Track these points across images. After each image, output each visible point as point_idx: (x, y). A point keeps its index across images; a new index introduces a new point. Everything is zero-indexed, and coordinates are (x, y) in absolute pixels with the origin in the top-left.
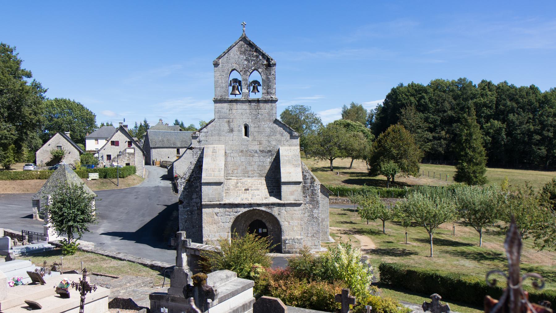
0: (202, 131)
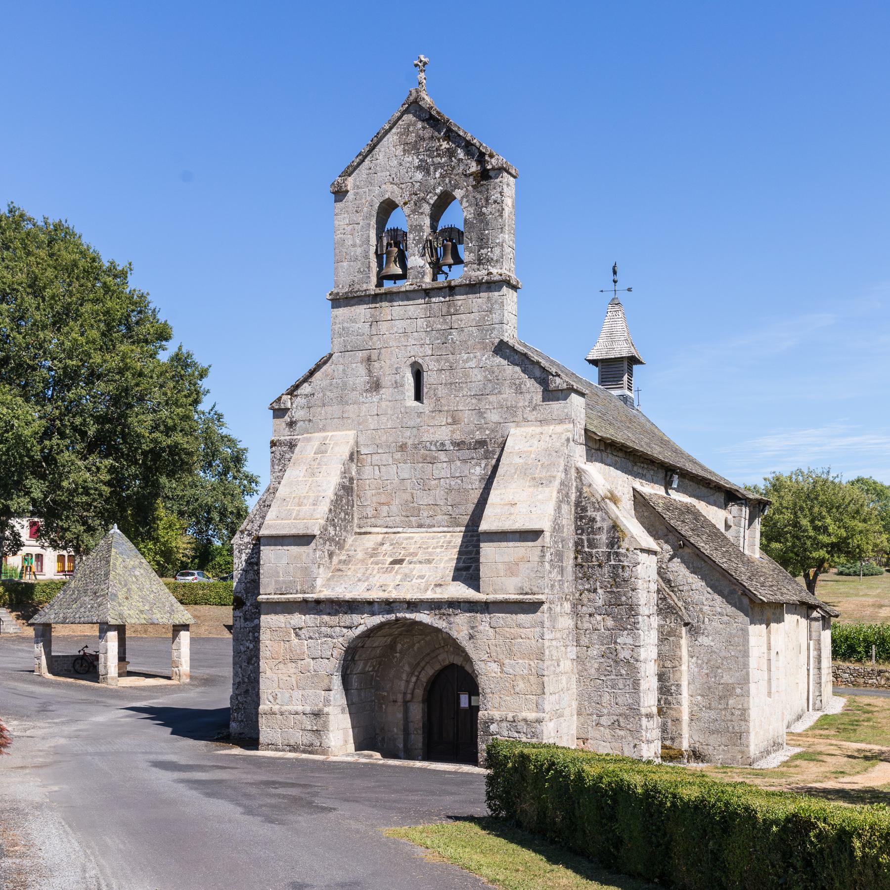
0: (299, 392)
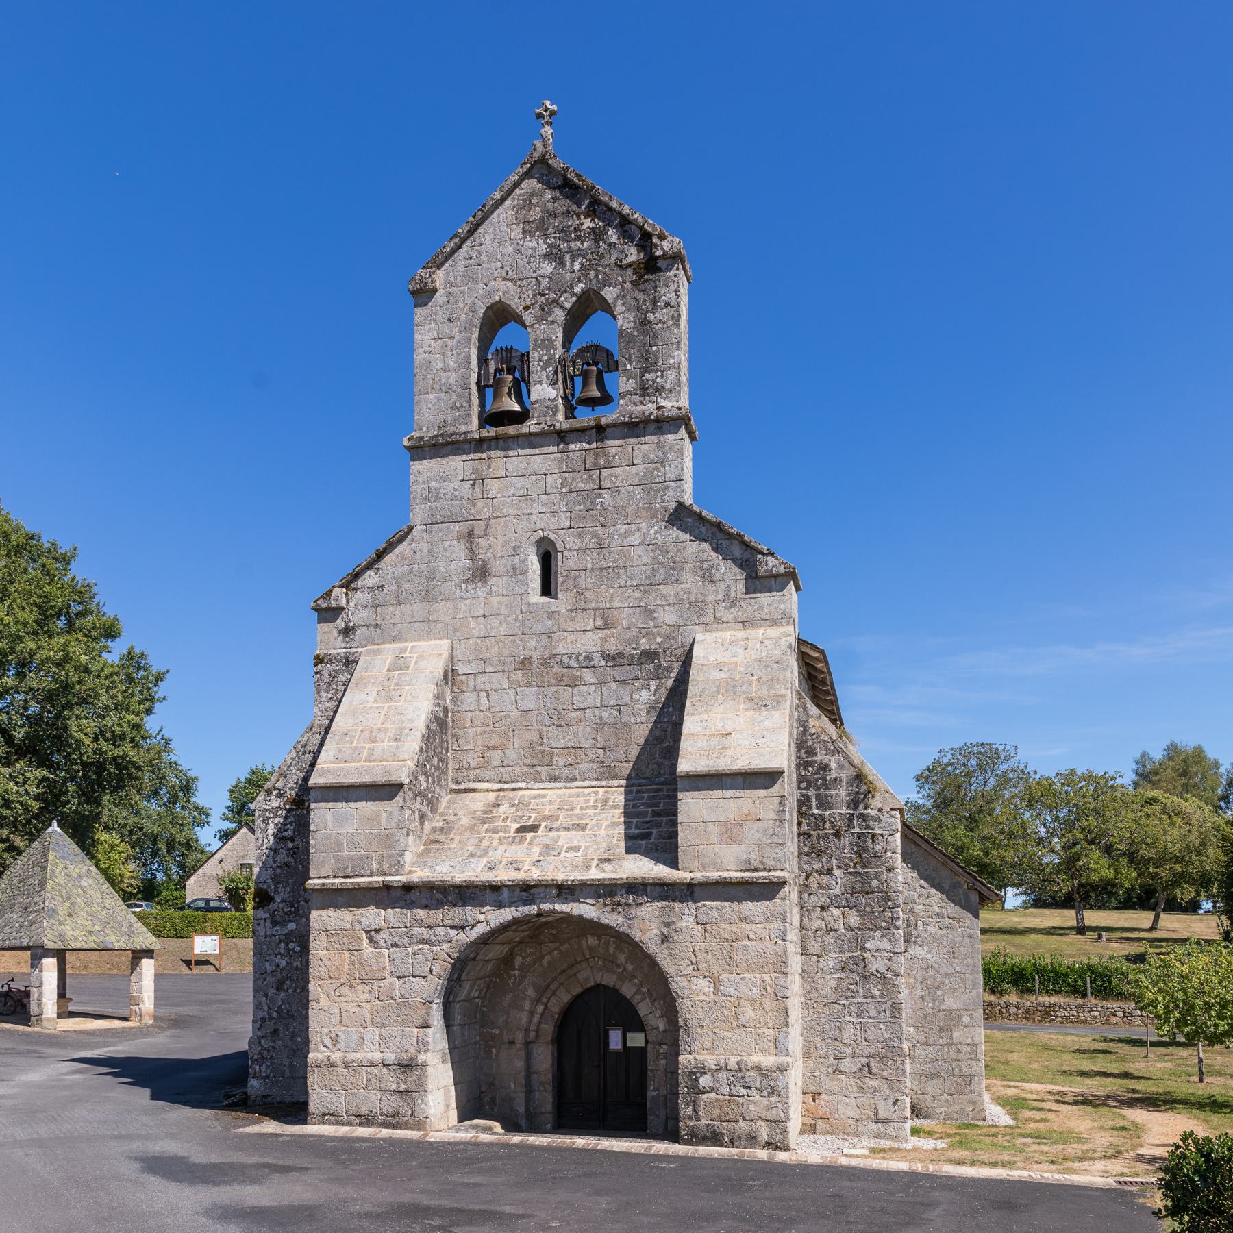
0: (359, 583)
